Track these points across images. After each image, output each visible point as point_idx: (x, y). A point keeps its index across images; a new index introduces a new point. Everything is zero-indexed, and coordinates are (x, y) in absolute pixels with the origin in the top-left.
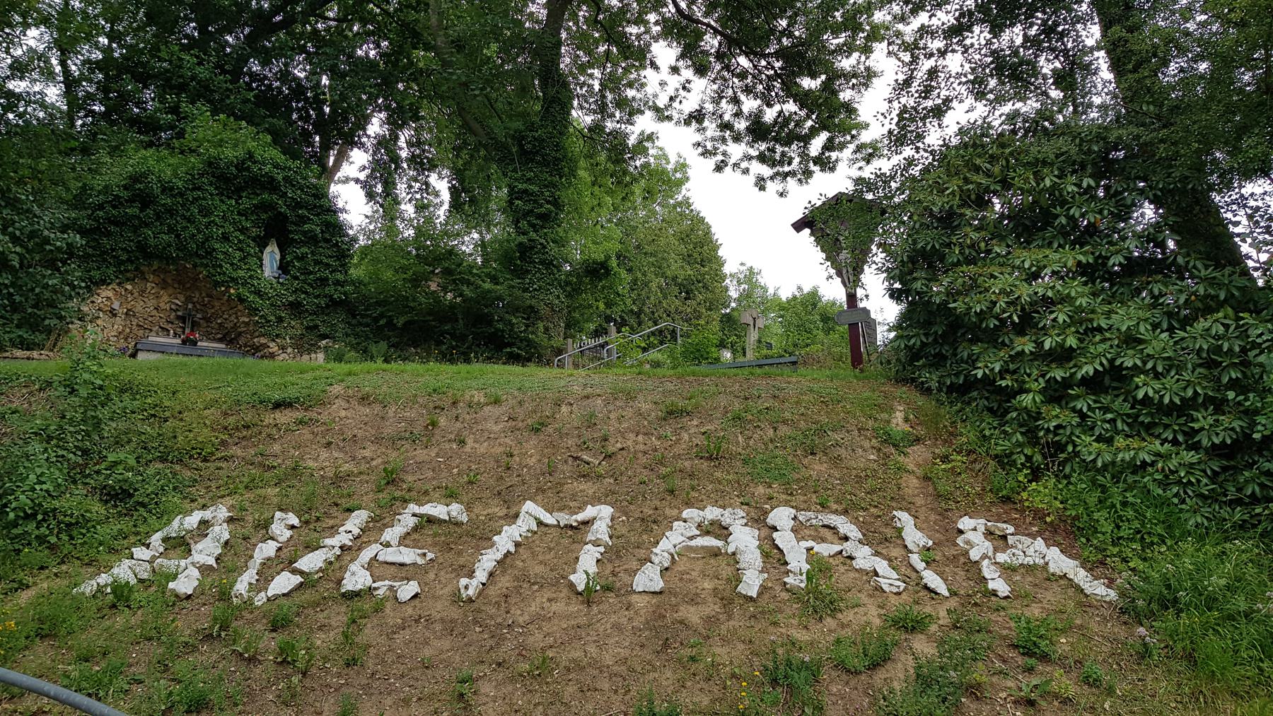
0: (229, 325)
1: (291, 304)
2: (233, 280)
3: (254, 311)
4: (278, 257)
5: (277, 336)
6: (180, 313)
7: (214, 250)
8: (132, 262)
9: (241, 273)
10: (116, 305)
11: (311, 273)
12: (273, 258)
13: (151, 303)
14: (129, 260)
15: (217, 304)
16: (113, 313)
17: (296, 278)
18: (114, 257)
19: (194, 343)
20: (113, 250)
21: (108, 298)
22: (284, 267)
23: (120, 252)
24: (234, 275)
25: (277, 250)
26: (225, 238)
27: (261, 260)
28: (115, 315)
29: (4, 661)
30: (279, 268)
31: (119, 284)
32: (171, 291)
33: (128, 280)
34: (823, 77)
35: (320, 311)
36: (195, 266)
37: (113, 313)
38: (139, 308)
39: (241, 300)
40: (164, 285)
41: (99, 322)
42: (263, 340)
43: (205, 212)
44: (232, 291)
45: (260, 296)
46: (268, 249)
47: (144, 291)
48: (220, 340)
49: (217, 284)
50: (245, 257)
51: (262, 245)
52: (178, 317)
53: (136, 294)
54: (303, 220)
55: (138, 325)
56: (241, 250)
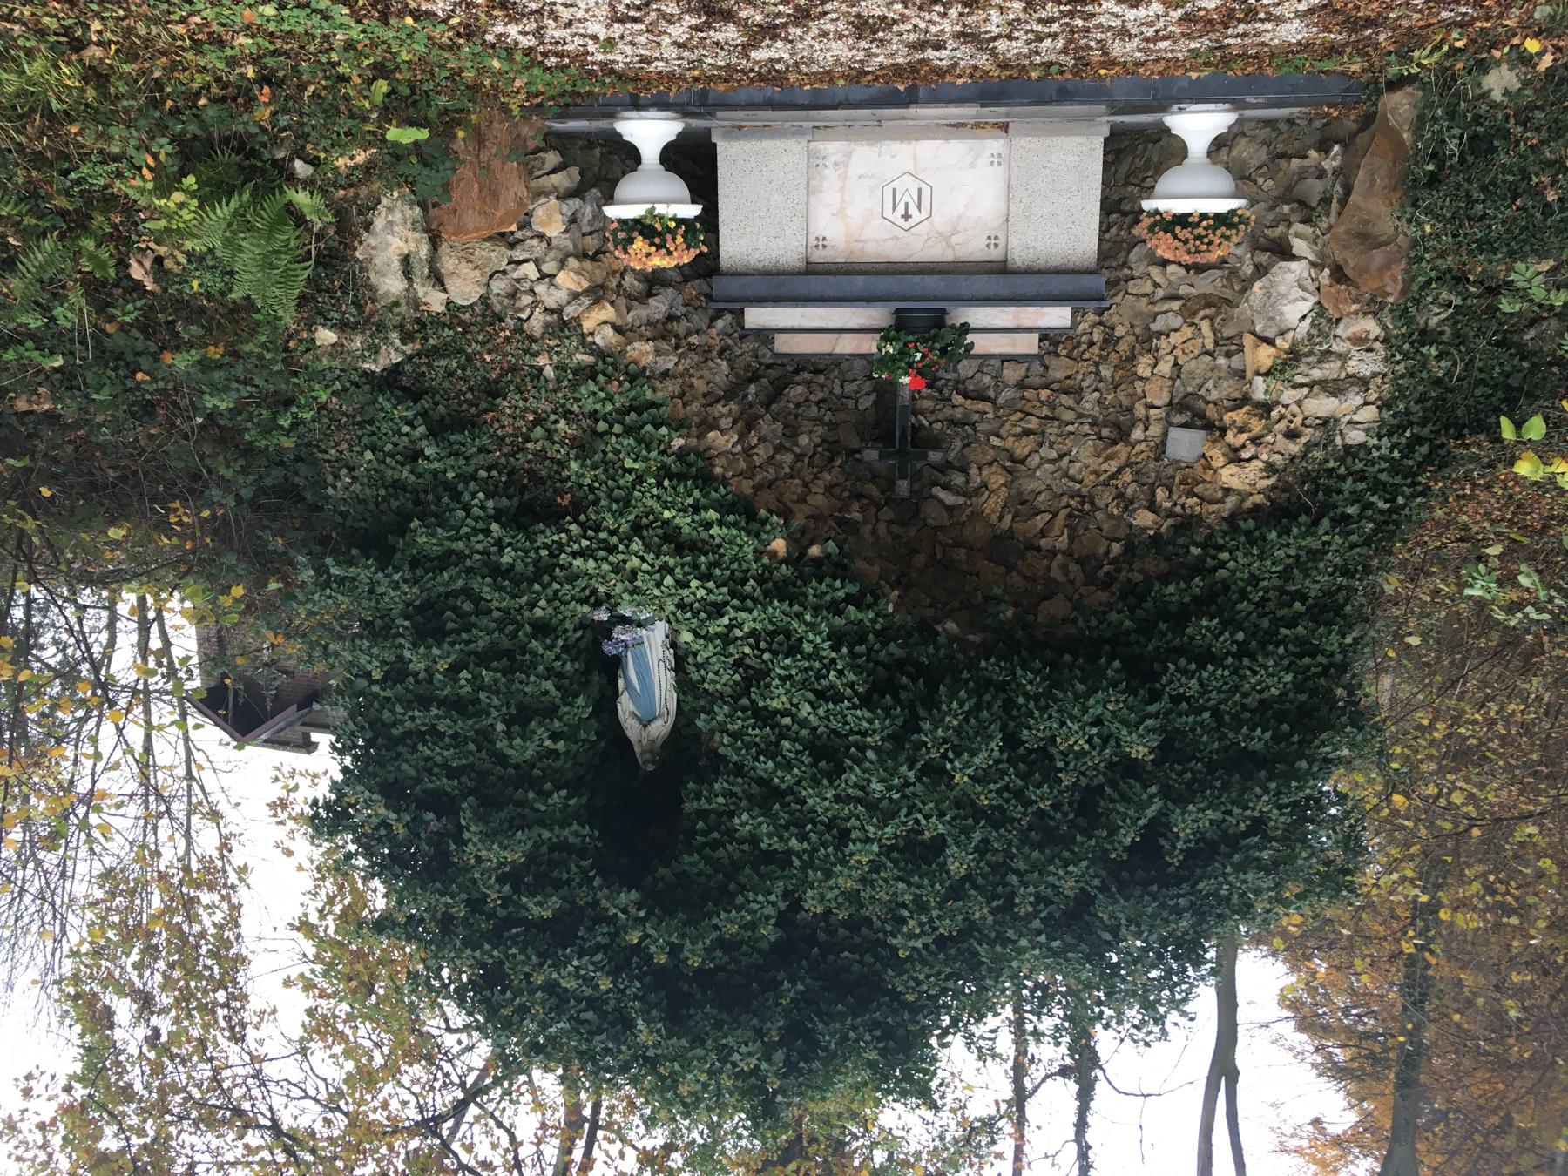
0: (768, 426)
1: (554, 517)
2: (783, 591)
3: (693, 471)
4: (625, 705)
5: (590, 373)
6: (935, 456)
7: (866, 701)
8: (1164, 613)
9: (750, 621)
10: (1185, 444)
11: (484, 659)
12: (644, 696)
13: (1041, 478)
14: (1180, 618)
17: (542, 629)
18: (1230, 623)
19: (902, 325)
20: (1243, 651)
21: (1234, 456)
22: (601, 668)
23: (1222, 643)
24: (777, 609)
25: (632, 728)
26: (829, 754)
27: (684, 684)
30: (613, 666)
34: (1552, 263)
35: (438, 497)
36: (927, 631)
37: (1191, 411)
39: (743, 511)
41: (1265, 356)
42: (642, 352)
43: (918, 854)
44: (779, 545)
45: (672, 539)
46: (660, 728)
49: (838, 568)
50: (745, 688)
51: (685, 747)
52: (936, 443)
54: (533, 875)
55: (1077, 392)
56: (765, 717)
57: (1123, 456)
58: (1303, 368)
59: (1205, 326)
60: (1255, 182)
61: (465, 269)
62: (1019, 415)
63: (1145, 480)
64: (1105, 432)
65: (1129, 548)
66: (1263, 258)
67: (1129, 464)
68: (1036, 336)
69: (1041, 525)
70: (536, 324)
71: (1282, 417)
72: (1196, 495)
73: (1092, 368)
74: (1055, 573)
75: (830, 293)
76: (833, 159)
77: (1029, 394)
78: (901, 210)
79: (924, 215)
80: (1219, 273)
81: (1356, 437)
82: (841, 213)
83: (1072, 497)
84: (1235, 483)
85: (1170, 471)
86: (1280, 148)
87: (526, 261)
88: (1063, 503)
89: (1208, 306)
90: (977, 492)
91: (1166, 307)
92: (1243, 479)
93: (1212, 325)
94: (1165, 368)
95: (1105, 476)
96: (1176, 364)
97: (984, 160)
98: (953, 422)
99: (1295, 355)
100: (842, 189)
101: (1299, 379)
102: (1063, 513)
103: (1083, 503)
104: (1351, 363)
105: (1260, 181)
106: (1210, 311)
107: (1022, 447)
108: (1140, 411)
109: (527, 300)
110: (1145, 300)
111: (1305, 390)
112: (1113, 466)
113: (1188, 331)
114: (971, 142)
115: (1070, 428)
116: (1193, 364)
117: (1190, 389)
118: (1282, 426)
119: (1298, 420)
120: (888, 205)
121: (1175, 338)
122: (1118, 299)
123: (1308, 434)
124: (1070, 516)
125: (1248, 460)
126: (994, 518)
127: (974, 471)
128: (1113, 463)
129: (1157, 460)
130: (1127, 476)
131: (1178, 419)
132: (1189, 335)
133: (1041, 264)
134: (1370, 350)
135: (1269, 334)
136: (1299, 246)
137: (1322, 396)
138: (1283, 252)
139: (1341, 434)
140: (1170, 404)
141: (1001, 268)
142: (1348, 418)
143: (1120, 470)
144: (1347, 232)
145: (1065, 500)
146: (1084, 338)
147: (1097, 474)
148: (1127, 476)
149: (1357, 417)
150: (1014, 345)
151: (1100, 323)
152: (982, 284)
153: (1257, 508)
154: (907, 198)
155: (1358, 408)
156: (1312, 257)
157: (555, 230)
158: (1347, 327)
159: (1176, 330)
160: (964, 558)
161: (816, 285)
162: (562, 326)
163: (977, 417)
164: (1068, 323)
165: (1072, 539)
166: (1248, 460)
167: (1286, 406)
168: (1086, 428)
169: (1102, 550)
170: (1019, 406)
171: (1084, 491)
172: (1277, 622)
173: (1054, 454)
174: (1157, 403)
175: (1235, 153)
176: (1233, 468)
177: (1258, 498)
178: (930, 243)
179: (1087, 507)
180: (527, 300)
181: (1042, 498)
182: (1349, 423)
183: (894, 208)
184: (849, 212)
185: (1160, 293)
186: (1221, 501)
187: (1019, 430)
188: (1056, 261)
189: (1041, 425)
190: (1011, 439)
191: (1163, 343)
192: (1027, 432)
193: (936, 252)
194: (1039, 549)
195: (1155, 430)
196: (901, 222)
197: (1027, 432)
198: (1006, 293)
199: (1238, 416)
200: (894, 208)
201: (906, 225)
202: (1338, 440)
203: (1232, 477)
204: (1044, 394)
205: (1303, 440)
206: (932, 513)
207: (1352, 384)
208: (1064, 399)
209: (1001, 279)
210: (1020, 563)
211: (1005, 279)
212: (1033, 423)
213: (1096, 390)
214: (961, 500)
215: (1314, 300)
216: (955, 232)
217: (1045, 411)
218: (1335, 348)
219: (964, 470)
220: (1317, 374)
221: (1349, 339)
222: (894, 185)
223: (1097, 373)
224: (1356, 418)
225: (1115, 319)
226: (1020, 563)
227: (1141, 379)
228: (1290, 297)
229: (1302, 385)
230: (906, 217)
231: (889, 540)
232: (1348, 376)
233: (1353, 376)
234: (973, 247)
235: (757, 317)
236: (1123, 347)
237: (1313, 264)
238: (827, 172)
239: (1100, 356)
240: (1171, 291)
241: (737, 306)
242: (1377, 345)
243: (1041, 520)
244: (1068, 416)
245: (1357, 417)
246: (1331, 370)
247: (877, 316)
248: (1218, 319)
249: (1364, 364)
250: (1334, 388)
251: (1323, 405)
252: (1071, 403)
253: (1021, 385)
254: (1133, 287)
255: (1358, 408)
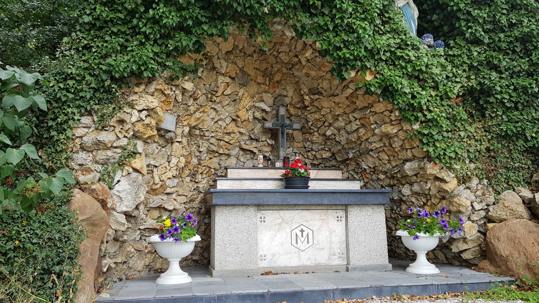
2: (372, 53)
6: (268, 125)
8: (188, 31)
10: (169, 122)
14: (181, 28)
15: (326, 104)
16: (165, 137)
17: (477, 42)
18: (155, 21)
21: (151, 111)
28: (171, 141)
29: (6, 63)
31: (171, 80)
32: (253, 88)
33: (185, 71)
37: (165, 137)
38: (208, 124)
40: (242, 79)
41: (138, 163)
47: (213, 92)
48: (337, 168)
53: (202, 99)
57: (193, 119)
58: (117, 156)
59: (157, 180)
60: (135, 249)
61: (514, 206)
62: (231, 142)
63: (185, 106)
64: (197, 132)
65: (195, 71)
66: (135, 213)
67: (191, 115)
68: (229, 176)
69: (229, 89)
70: (475, 181)
71: (127, 131)
72: (165, 95)
73: (202, 162)
74: (224, 64)
75: (339, 196)
76: (336, 257)
77: (227, 152)
78: (305, 234)
79: (294, 232)
80: (152, 205)
81: (86, 120)
82: (332, 232)
83: (215, 101)
84: (150, 98)
85: (175, 110)
86: (125, 267)
87: (479, 210)
88: (219, 98)
89: (155, 190)
90: (251, 107)
91: (173, 190)
92: (145, 99)
93: (154, 180)
94: (174, 161)
95: (201, 110)
96: (169, 162)
97: (268, 257)
98: (257, 140)
99: (121, 164)
100: (331, 243)
101: (119, 151)
102: (219, 94)
103: (211, 98)
104: (90, 158)
105: (133, 250)
106: (155, 187)
107: (232, 127)
108: (184, 140)
109: (479, 193)
110: (180, 193)
111: (115, 145)
112: (198, 115)
113: (164, 177)
114: (275, 265)
115: (213, 135)
116: (162, 162)
117: (164, 149)
118: (127, 127)
119: (117, 130)
120: (310, 236)
121: (170, 174)
122: (191, 194)
123: (113, 122)
124: (217, 92)
125: (144, 110)
126: (246, 95)
127: (251, 118)
128: (198, 116)
129: (179, 116)
130: (192, 109)
131: (171, 135)
132: (163, 176)
133: (241, 209)
134: (81, 165)
135: (134, 175)
136: (122, 219)
137: (107, 141)
138: (128, 216)
139: (94, 121)
140: (172, 143)
141: (259, 206)
142: (91, 130)
143: (195, 112)
144: (101, 226)
145: (218, 101)
146: (204, 176)
147: (204, 112)
148: (192, 109)
149: (84, 130)
150: (238, 173)
151: (197, 183)
152: (271, 199)
153: (138, 85)
154: (302, 239)
155: (85, 135)
156: (114, 213)
157: (467, 224)
158: (94, 178)
159: (169, 178)
160: (259, 77)
161: (345, 200)
162: (463, 180)
163: (248, 142)
164: (218, 182)
165: (216, 80)
166: (144, 110)
167: (125, 137)
168: (207, 134)
169: (205, 73)
170: (231, 146)
171: (210, 103)
172: (125, 22)
173: (220, 122)
174: (177, 144)
175: (143, 262)
176: (152, 106)
177: (137, 89)
178: (291, 219)
179: (209, 96)
180: (479, 193)
181: (227, 102)
182: (90, 128)
183: (308, 235)
184: (328, 233)
185: (174, 196)
186: (156, 90)
187: (232, 135)
188: (236, 209)
189: (223, 137)
190: (236, 131)
191: (175, 173)
192: (229, 134)
193: (288, 214)
194: (230, 77)
195: (179, 131)
196: (304, 229)
197: (229, 134)
198: (260, 195)
199: (150, 133)
200: (308, 235)
201: (302, 227)
202: (96, 119)
203: (153, 102)
204: (221, 151)
205: (114, 119)
206: (269, 98)
207: (90, 147)
208: (215, 149)
209: (261, 202)
210: (238, 72)
211: (258, 201)
212: (227, 138)
213: (200, 152)
214: (257, 105)
215: (114, 191)
216: (280, 224)
217: (222, 143)
218: (100, 167)
219: (255, 118)
220: (109, 153)
221: (92, 171)
222: (308, 245)
223: (200, 160)
224: (86, 130)
225: (190, 185)
226: (238, 72)
227: (184, 156)
228: (125, 192)
229: (116, 147)
230: (302, 231)
231: (288, 88)
232: (92, 151)
233: (88, 151)
234: (271, 216)
235: (355, 186)
236: (187, 172)
237: (114, 209)
238: (338, 251)
239: (198, 168)
240: (170, 197)
241: (365, 190)
242: (77, 167)
243: (228, 91)
244: (213, 140)
245: (84, 130)
246: (101, 155)
247: (313, 186)
248: (152, 183)
249: (82, 157)
250: (99, 145)
251: (106, 137)
252: (212, 146)
253: (229, 155)
254: (183, 199)
255: (85, 135)
